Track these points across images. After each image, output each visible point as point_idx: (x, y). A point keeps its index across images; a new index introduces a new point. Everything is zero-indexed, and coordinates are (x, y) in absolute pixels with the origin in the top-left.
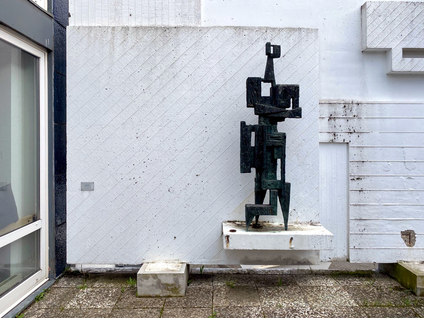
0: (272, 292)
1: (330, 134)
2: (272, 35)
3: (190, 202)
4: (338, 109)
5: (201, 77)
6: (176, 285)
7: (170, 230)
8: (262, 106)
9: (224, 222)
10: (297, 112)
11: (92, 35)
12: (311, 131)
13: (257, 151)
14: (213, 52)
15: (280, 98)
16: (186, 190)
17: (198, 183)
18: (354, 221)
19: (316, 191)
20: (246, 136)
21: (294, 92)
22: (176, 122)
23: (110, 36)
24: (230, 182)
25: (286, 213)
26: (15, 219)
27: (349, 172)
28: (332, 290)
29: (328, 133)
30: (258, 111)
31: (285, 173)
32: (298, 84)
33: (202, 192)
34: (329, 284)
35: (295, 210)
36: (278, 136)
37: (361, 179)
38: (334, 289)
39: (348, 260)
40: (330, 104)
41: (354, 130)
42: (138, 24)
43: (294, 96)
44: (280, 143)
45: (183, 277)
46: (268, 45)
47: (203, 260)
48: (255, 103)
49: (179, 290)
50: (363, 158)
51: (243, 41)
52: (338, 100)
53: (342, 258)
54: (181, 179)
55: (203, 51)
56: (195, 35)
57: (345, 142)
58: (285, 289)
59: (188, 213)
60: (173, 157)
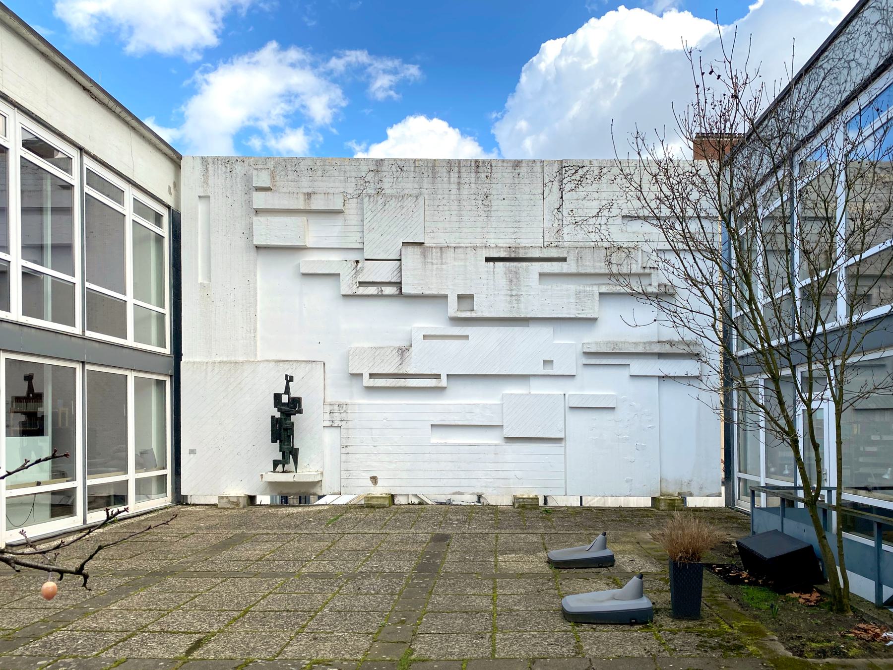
11: (195, 366)
46: (287, 376)
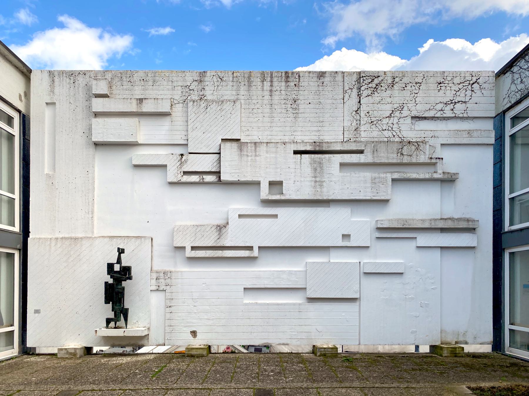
2: (127, 241)
11: (40, 242)
18: (167, 327)
19: (148, 312)
23: (49, 242)
26: (3, 324)
42: (63, 236)
46: (119, 249)
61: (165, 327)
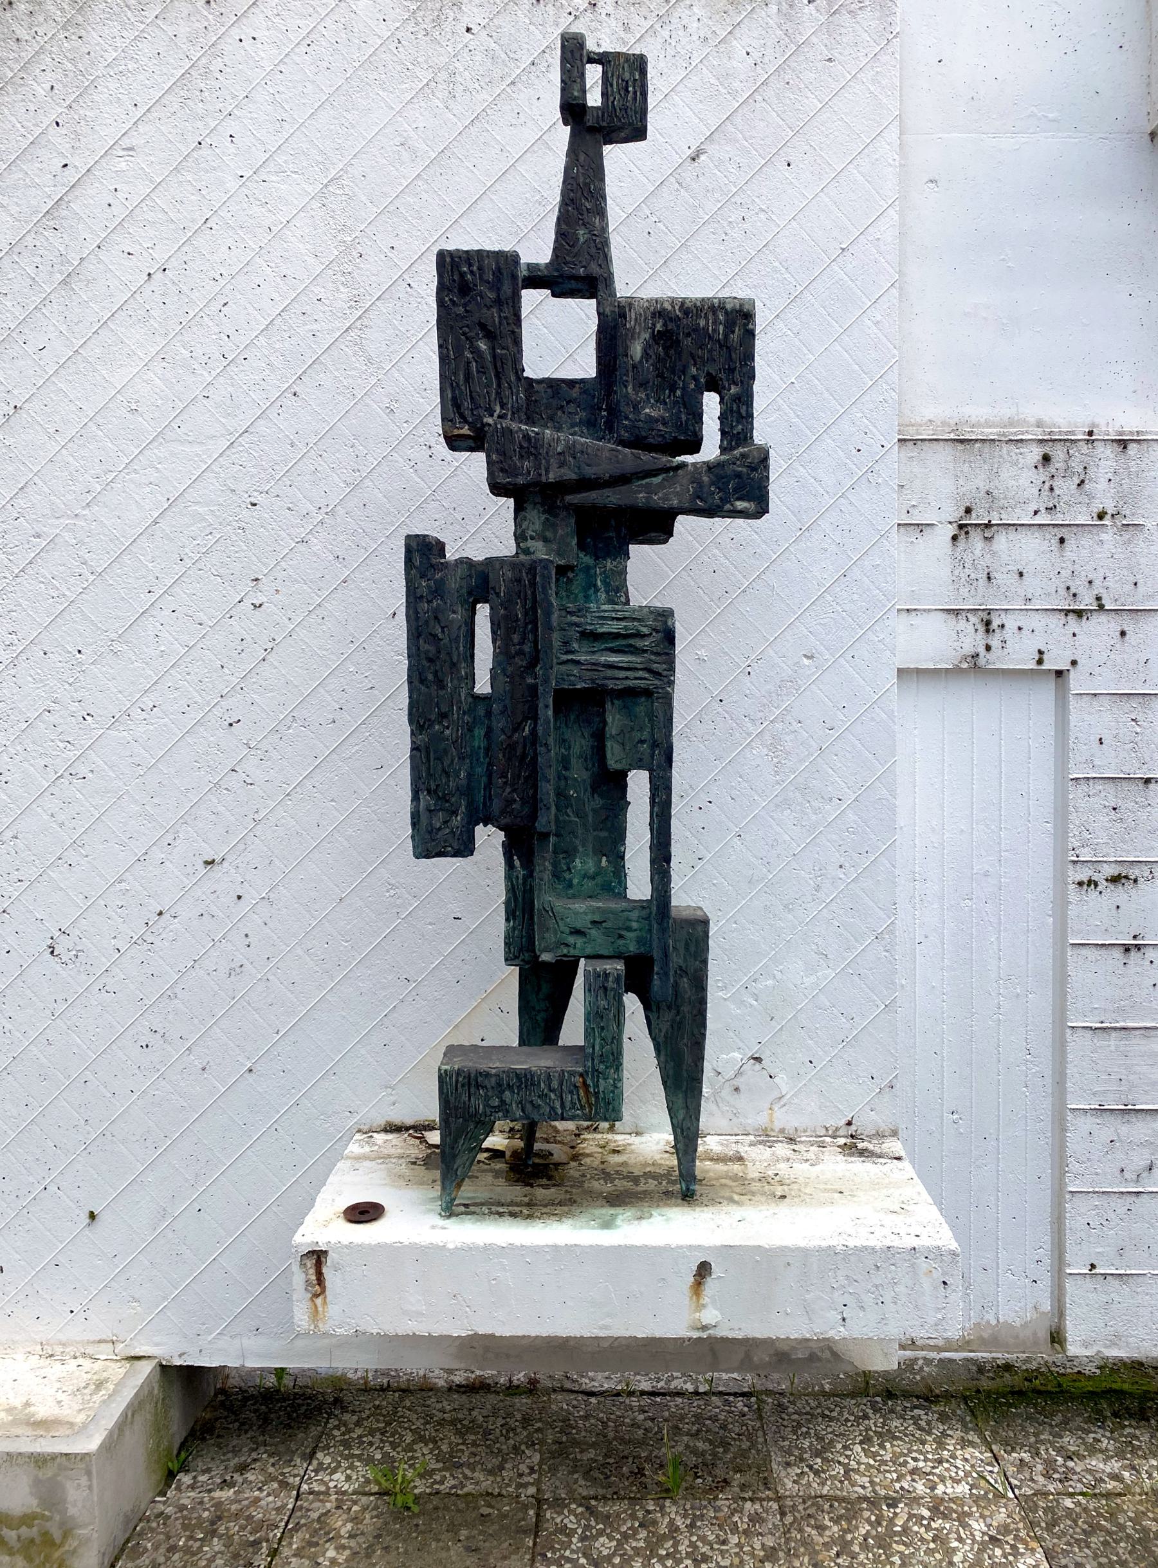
0: (614, 1554)
1: (962, 624)
2: (626, 28)
3: (170, 1017)
4: (1006, 473)
5: (222, 282)
6: (49, 1519)
7: (61, 1173)
8: (526, 437)
9: (366, 1128)
10: (738, 475)
12: (853, 601)
13: (499, 723)
14: (288, 129)
15: (641, 385)
16: (147, 946)
17: (214, 910)
20: (438, 631)
21: (724, 345)
22: (83, 552)
24: (398, 902)
25: (686, 1098)
27: (1065, 832)
28: (960, 1539)
29: (952, 617)
30: (502, 470)
31: (668, 859)
32: (739, 291)
33: (240, 959)
34: (949, 1483)
35: (758, 1060)
36: (625, 628)
37: (1135, 881)
38: (975, 1525)
39: (1057, 1338)
40: (960, 447)
41: (1099, 599)
43: (722, 375)
44: (640, 674)
45: (89, 1473)
47: (251, 1343)
48: (480, 418)
49: (67, 1548)
50: (1147, 759)
51: (457, 64)
52: (1011, 423)
53: (1025, 1326)
54: (118, 887)
55: (232, 126)
56: (183, 30)
57: (1045, 667)
58: (692, 1525)
59: (162, 1077)
60: (72, 754)
61: (1063, 1129)
